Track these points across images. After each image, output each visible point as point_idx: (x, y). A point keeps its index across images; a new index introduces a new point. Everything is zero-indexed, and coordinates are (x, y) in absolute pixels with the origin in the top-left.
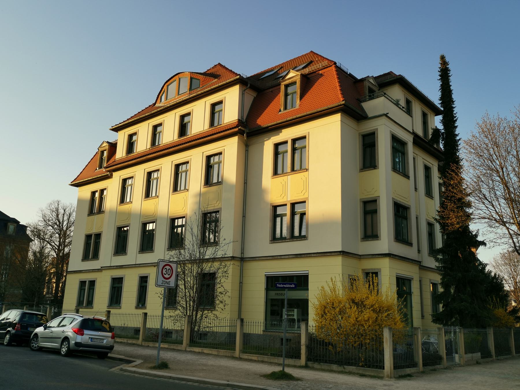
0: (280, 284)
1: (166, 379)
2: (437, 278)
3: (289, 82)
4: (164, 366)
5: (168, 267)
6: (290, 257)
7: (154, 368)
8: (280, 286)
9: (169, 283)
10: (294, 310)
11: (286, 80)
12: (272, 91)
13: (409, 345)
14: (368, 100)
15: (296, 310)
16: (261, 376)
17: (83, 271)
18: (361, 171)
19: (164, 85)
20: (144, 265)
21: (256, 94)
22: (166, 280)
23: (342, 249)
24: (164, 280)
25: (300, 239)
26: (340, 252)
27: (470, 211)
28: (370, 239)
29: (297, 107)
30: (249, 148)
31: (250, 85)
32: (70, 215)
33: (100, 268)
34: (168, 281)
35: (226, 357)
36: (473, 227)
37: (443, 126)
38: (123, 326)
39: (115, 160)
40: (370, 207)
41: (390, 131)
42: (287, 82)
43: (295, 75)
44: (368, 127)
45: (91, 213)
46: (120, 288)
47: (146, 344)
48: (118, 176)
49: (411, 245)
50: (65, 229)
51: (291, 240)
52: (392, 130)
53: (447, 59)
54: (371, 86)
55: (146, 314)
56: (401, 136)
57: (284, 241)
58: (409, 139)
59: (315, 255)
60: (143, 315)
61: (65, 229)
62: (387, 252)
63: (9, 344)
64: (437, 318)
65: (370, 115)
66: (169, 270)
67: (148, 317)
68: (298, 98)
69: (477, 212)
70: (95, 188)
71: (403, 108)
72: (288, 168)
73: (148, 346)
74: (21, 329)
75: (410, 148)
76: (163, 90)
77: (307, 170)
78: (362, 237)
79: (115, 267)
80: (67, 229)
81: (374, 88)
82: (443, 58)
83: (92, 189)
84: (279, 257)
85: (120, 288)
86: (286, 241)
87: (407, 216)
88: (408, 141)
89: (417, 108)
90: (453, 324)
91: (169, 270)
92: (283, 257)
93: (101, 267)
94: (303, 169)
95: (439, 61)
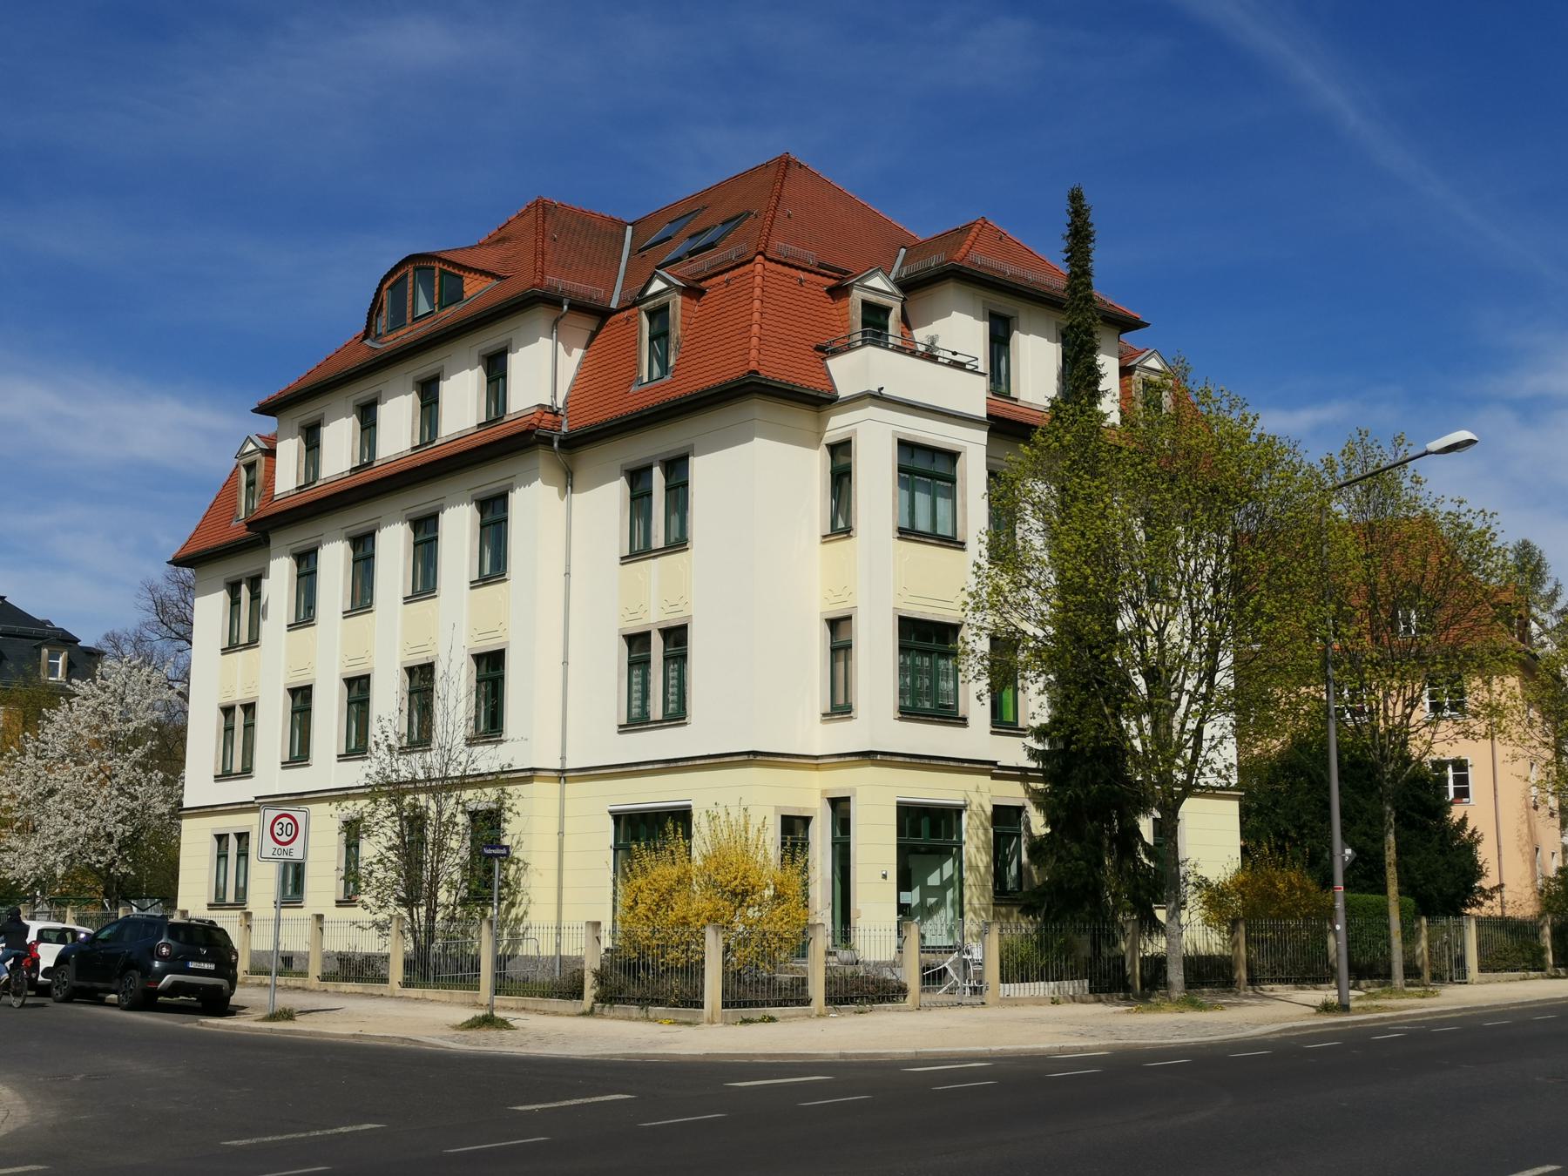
4: (288, 1015)
5: (285, 820)
7: (265, 1019)
12: (627, 319)
14: (860, 343)
16: (452, 1027)
21: (597, 322)
22: (282, 847)
24: (278, 846)
30: (574, 478)
33: (253, 799)
35: (463, 1004)
38: (1037, 993)
44: (838, 425)
47: (330, 986)
53: (1088, 200)
54: (873, 298)
56: (944, 439)
60: (315, 918)
65: (844, 391)
66: (289, 826)
73: (326, 991)
82: (1076, 197)
91: (289, 826)
93: (256, 798)
95: (1065, 205)
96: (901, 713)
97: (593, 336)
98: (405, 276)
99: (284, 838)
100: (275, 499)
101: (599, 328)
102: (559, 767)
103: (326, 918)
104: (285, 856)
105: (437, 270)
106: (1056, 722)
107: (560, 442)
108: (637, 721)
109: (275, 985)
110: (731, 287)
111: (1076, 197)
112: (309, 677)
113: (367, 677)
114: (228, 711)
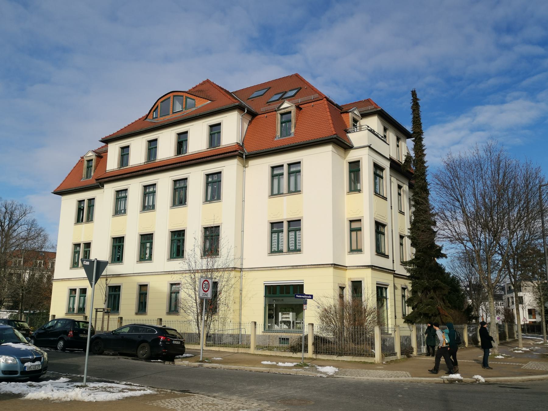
0: (299, 295)
1: (345, 354)
2: (408, 284)
3: (284, 111)
5: (206, 282)
6: (287, 268)
8: (298, 296)
9: (207, 295)
10: (289, 314)
11: (281, 109)
13: (326, 342)
15: (291, 313)
17: (72, 279)
18: (348, 193)
19: (158, 100)
20: (141, 274)
22: (205, 293)
23: (333, 262)
25: (296, 253)
26: (332, 264)
27: (435, 229)
28: (355, 253)
29: (292, 136)
31: (247, 110)
32: (11, 213)
34: (206, 293)
36: (438, 243)
37: (414, 154)
39: (106, 171)
40: (355, 225)
41: (373, 160)
42: (282, 111)
43: (290, 106)
44: (353, 155)
45: (272, 195)
46: (117, 295)
48: (110, 189)
49: (387, 257)
50: (6, 228)
51: (288, 253)
52: (374, 159)
54: (355, 117)
55: (121, 318)
56: (381, 163)
57: (281, 254)
58: (386, 165)
59: (310, 267)
61: (6, 228)
62: (370, 264)
63: (63, 349)
64: (409, 320)
65: (355, 145)
67: (123, 321)
68: (293, 127)
69: (442, 232)
70: (82, 198)
71: (382, 137)
72: (285, 189)
74: (73, 335)
75: (387, 173)
76: (156, 106)
77: (300, 191)
78: (349, 251)
79: (111, 276)
80: (9, 228)
81: (357, 118)
83: (78, 198)
84: (277, 268)
85: (117, 295)
86: (283, 254)
87: (384, 232)
88: (386, 166)
89: (391, 136)
90: (420, 323)
92: (280, 268)
94: (297, 191)
96: (377, 253)
97: (250, 122)
98: (169, 98)
99: (206, 289)
100: (107, 172)
101: (252, 119)
102: (240, 268)
103: (163, 320)
104: (206, 297)
105: (184, 97)
106: (416, 258)
107: (246, 156)
108: (275, 251)
109: (203, 350)
110: (314, 108)
111: (414, 93)
112: (152, 230)
113: (123, 238)
114: (77, 245)
